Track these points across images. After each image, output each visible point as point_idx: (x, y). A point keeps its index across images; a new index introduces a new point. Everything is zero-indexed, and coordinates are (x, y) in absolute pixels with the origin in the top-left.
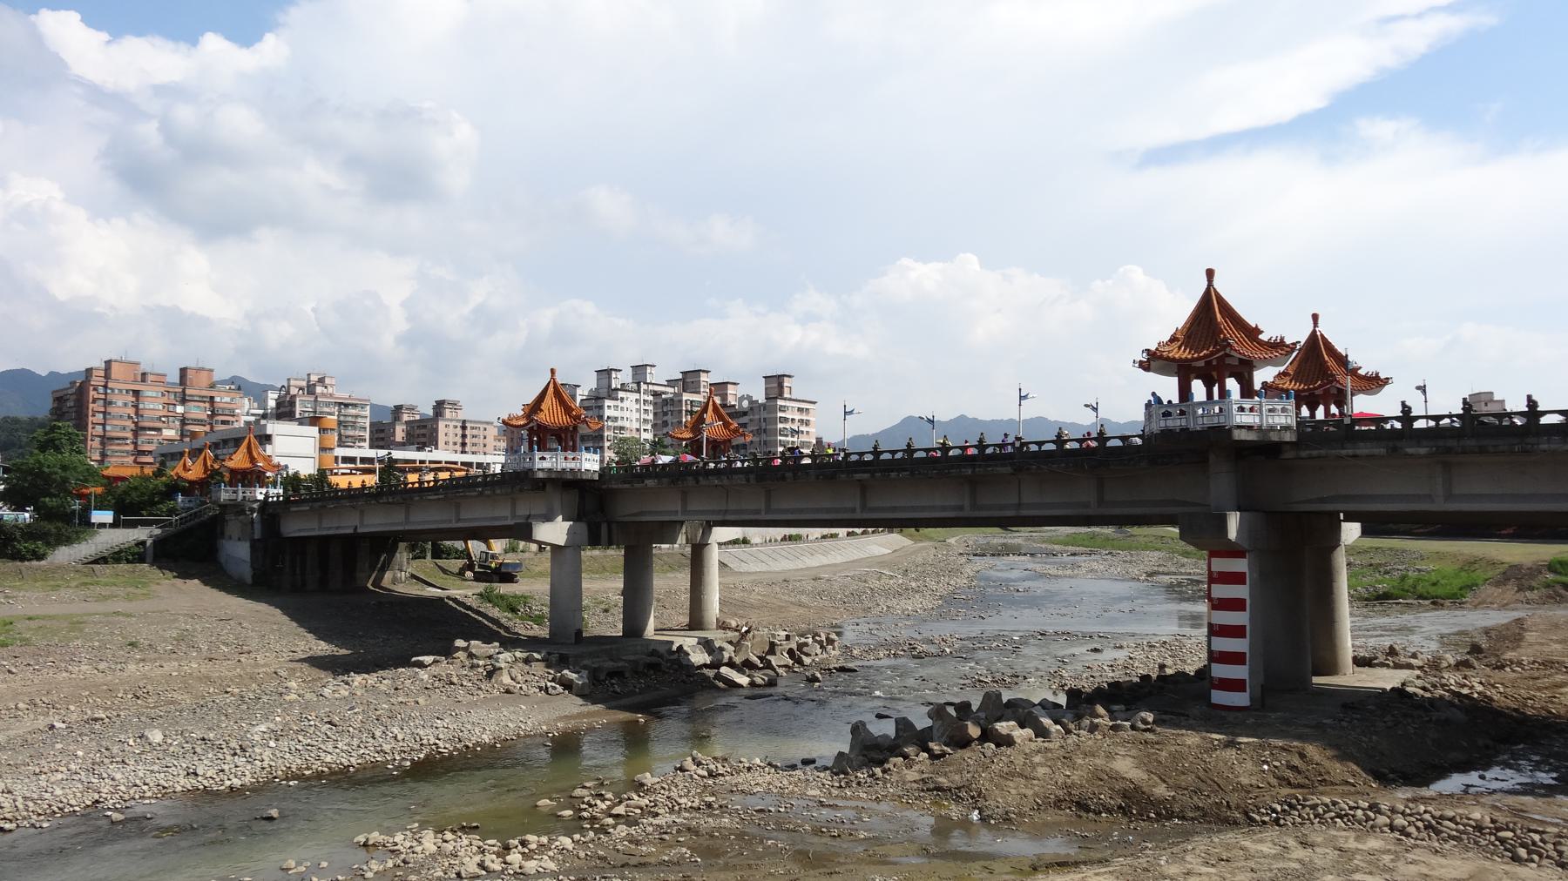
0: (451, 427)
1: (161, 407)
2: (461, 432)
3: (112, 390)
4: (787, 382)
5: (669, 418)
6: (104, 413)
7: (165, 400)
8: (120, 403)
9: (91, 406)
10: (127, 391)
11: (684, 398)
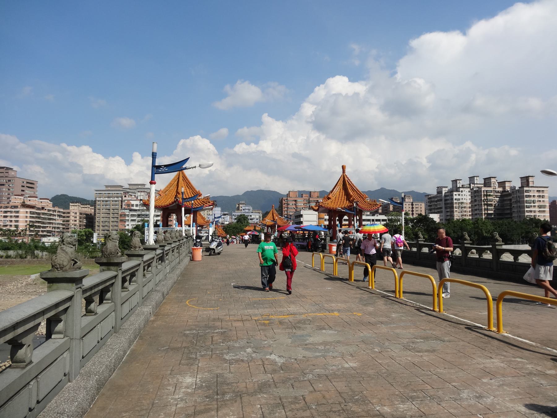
0: (407, 205)
1: (303, 205)
2: (411, 207)
3: (289, 200)
4: (531, 179)
5: (477, 198)
6: (287, 207)
7: (304, 202)
8: (291, 204)
9: (283, 205)
10: (293, 200)
11: (483, 190)
